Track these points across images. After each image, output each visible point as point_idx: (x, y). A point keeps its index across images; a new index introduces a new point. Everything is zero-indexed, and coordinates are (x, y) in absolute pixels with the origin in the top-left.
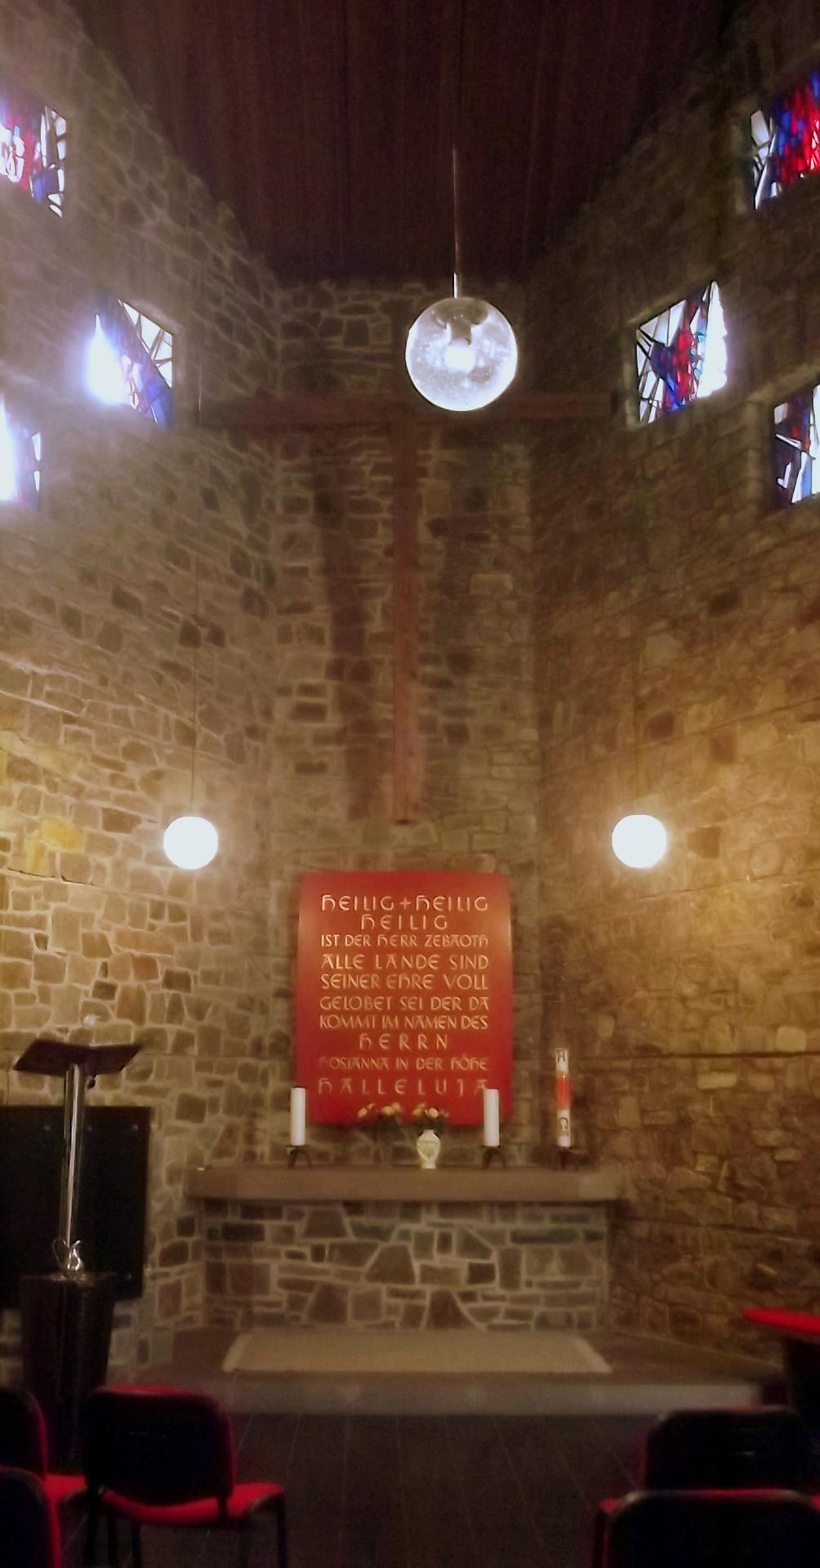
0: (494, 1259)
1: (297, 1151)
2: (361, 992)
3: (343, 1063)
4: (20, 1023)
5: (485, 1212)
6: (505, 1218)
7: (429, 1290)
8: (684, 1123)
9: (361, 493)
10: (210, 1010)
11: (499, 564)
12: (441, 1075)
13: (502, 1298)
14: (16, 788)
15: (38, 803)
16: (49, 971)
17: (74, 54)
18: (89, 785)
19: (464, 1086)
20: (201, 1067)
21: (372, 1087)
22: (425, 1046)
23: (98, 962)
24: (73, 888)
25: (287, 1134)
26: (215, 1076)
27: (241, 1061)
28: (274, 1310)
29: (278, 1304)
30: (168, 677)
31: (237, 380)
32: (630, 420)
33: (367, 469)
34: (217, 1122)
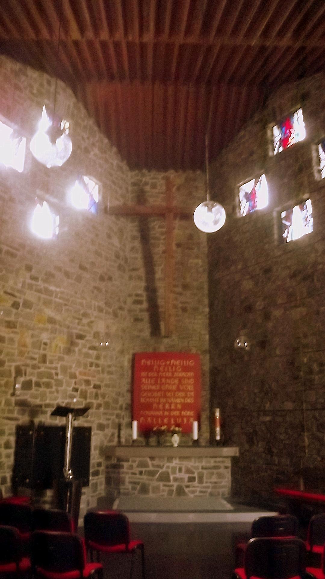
0: (196, 475)
1: (134, 441)
4: (51, 399)
5: (193, 460)
7: (176, 484)
8: (255, 432)
10: (107, 396)
11: (197, 257)
12: (179, 417)
13: (198, 487)
14: (50, 326)
15: (56, 331)
16: (59, 383)
17: (72, 105)
18: (71, 325)
20: (105, 414)
21: (157, 420)
23: (74, 381)
24: (66, 357)
25: (131, 435)
26: (108, 417)
27: (116, 412)
28: (126, 491)
29: (128, 489)
30: (95, 291)
31: (117, 199)
32: (238, 214)
33: (157, 227)
34: (109, 431)
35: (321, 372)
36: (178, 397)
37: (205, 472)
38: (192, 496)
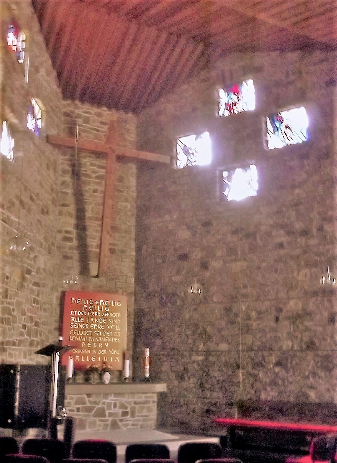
0: (129, 410)
2: (83, 329)
3: (76, 351)
5: (127, 396)
6: (132, 398)
7: (111, 419)
8: (186, 370)
9: (85, 171)
12: (105, 355)
13: (130, 420)
19: (112, 359)
21: (85, 359)
22: (101, 347)
32: (175, 165)
33: (88, 164)
35: (258, 319)
36: (106, 336)
37: (137, 406)
38: (125, 429)
